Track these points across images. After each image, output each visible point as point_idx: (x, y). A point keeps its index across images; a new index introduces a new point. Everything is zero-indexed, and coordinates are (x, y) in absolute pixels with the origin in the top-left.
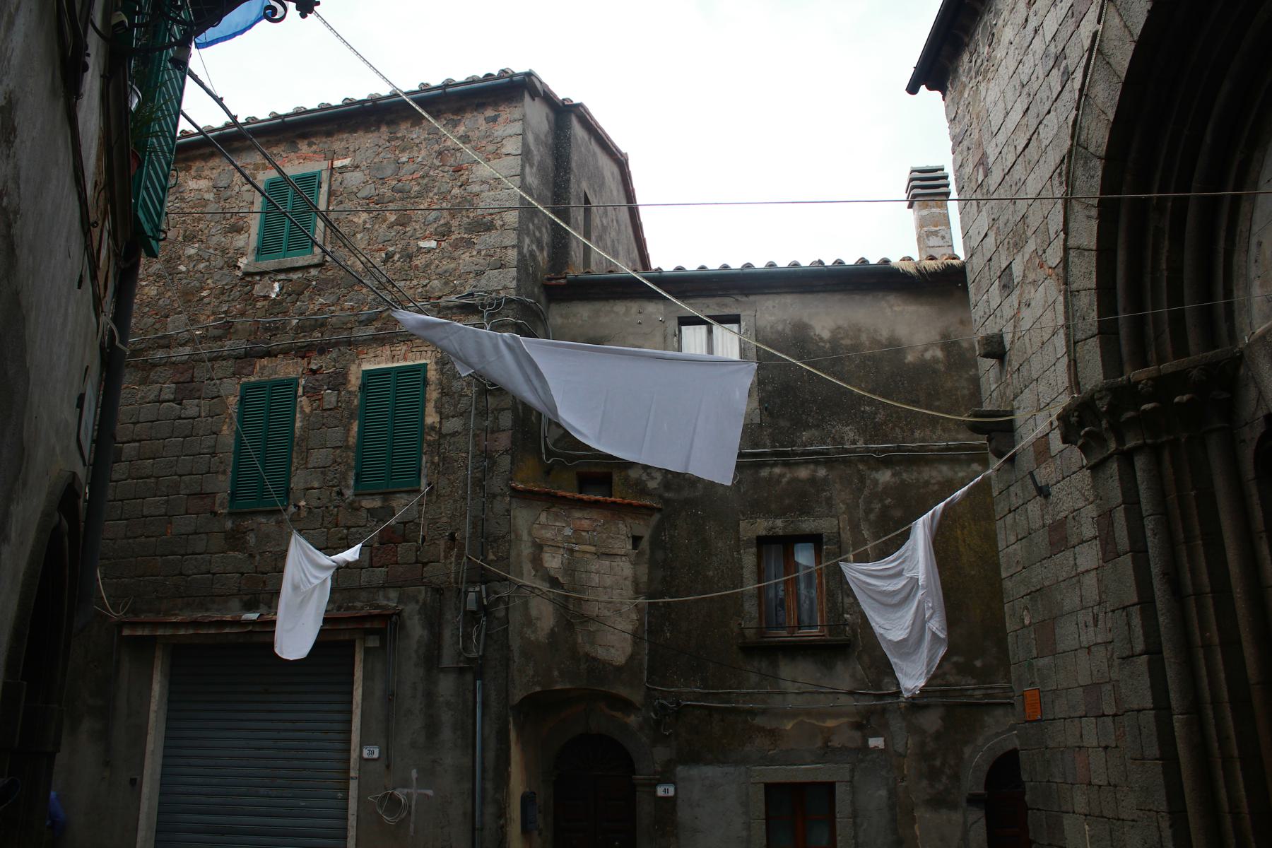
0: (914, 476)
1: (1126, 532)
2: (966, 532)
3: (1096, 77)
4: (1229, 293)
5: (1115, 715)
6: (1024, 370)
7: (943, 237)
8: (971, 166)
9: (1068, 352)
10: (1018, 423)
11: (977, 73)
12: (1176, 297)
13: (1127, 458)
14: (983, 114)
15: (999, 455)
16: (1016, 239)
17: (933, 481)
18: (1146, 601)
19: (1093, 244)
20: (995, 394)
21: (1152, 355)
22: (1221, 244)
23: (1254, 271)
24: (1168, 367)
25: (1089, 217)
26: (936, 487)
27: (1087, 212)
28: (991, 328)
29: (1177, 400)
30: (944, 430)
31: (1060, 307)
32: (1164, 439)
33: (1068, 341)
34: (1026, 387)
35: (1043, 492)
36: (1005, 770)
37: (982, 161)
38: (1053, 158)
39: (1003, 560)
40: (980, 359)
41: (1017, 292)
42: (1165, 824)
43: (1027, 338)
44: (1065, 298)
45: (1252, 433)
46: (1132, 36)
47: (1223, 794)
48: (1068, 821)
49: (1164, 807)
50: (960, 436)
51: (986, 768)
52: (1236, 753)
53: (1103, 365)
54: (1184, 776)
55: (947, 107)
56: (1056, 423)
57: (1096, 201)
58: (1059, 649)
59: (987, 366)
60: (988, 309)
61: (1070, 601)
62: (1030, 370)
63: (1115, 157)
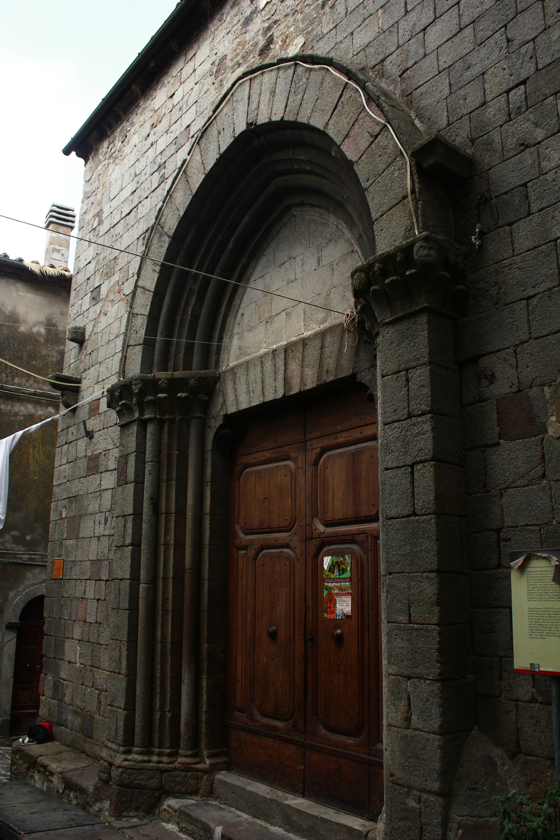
0: (9, 407)
1: (133, 470)
2: (36, 450)
3: (179, 186)
4: (221, 339)
5: (107, 581)
6: (94, 354)
7: (63, 255)
8: (92, 216)
9: (123, 350)
10: (82, 389)
11: (110, 157)
12: (192, 335)
13: (143, 424)
14: (107, 184)
15: (67, 406)
16: (108, 270)
17: (20, 414)
18: (137, 514)
19: (152, 288)
20: (72, 366)
21: (171, 365)
22: (223, 308)
23: (236, 330)
24: (178, 374)
25: (154, 271)
26: (22, 418)
27: (153, 267)
28: (79, 323)
29: (179, 395)
30: (34, 381)
31: (124, 321)
32: (167, 417)
33: (124, 344)
34: (92, 366)
35: (89, 435)
36: (35, 607)
37: (99, 214)
38: (143, 226)
39: (56, 474)
40: (67, 341)
41: (100, 304)
42: (124, 649)
43: (100, 335)
44: (129, 316)
45: (216, 423)
46: (205, 170)
47: (159, 632)
48: (68, 644)
49: (125, 638)
50: (45, 387)
51: (22, 606)
52: (170, 608)
53: (141, 364)
54: (140, 620)
55: (86, 171)
56: (106, 393)
57: (160, 264)
58: (81, 536)
59: (71, 347)
60: (79, 310)
61: (93, 506)
62: (97, 356)
63: (177, 239)
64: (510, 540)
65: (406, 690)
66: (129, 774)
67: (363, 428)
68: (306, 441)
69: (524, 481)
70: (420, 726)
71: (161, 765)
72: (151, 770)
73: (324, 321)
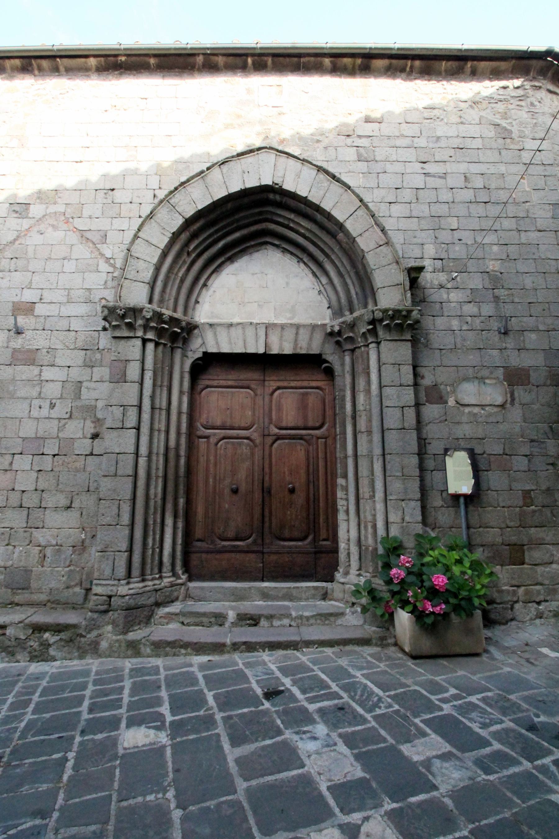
32: (163, 342)
66: (134, 599)
69: (438, 421)
70: (410, 521)
71: (156, 587)
73: (290, 319)
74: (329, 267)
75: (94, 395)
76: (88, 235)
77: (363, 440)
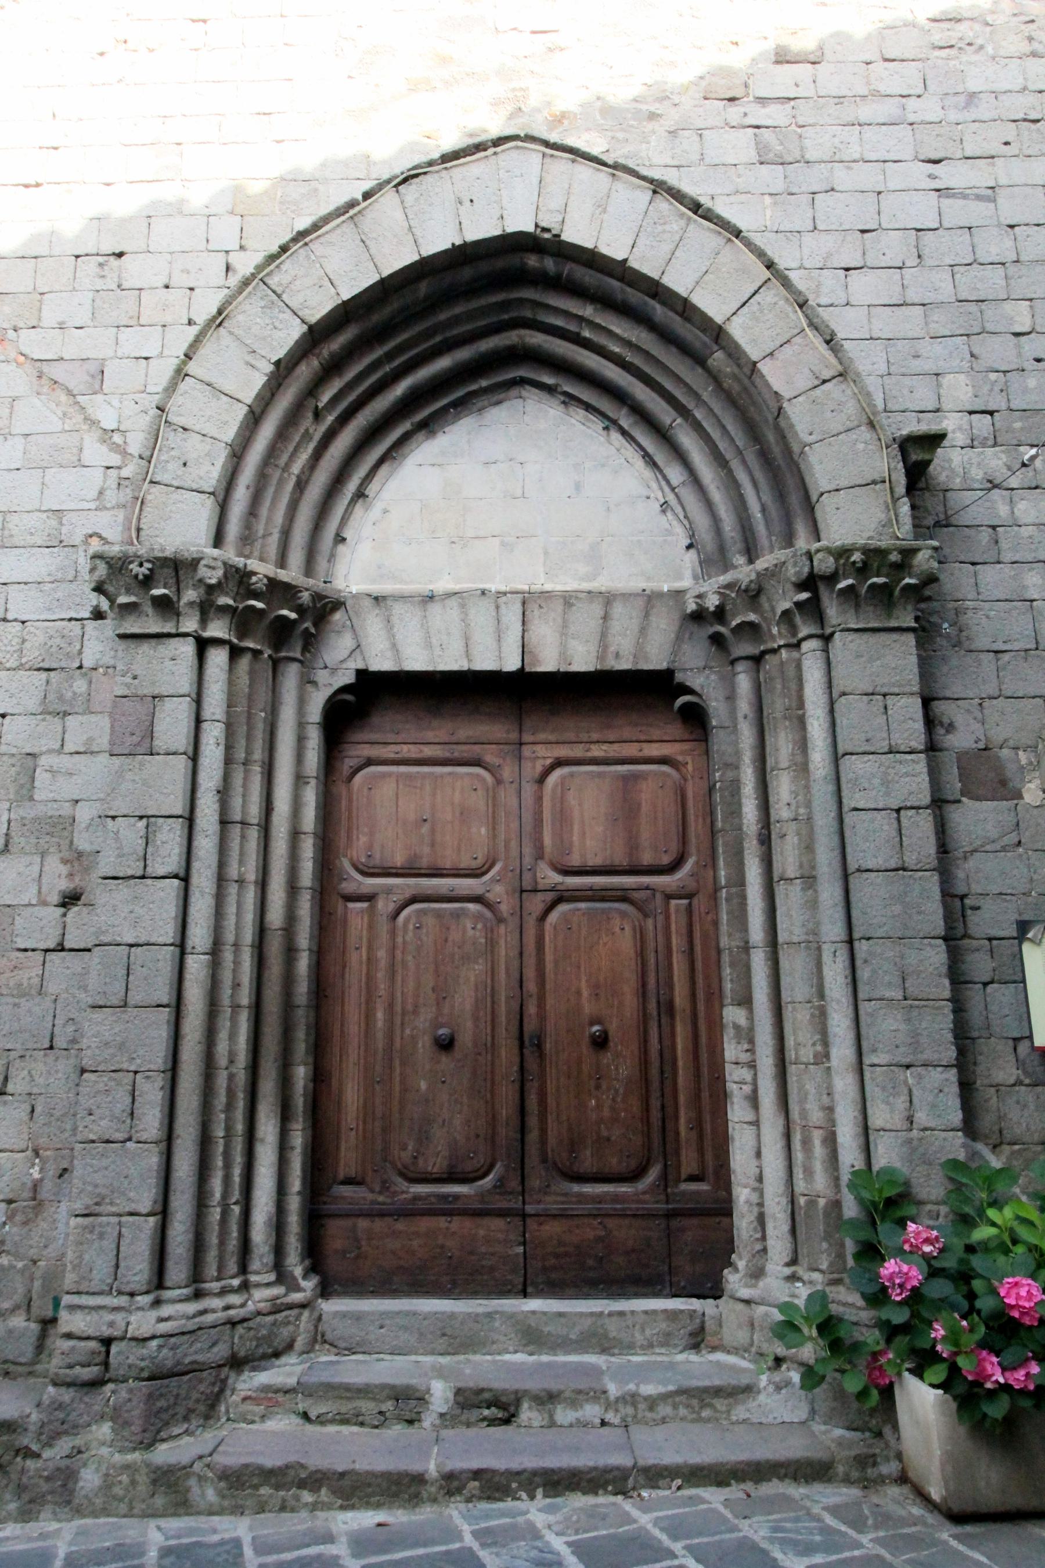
32: (251, 645)
64: (978, 908)
65: (906, 1082)
67: (644, 745)
68: (521, 744)
72: (215, 1327)
74: (687, 440)
75: (68, 789)
76: (57, 372)
77: (791, 900)
